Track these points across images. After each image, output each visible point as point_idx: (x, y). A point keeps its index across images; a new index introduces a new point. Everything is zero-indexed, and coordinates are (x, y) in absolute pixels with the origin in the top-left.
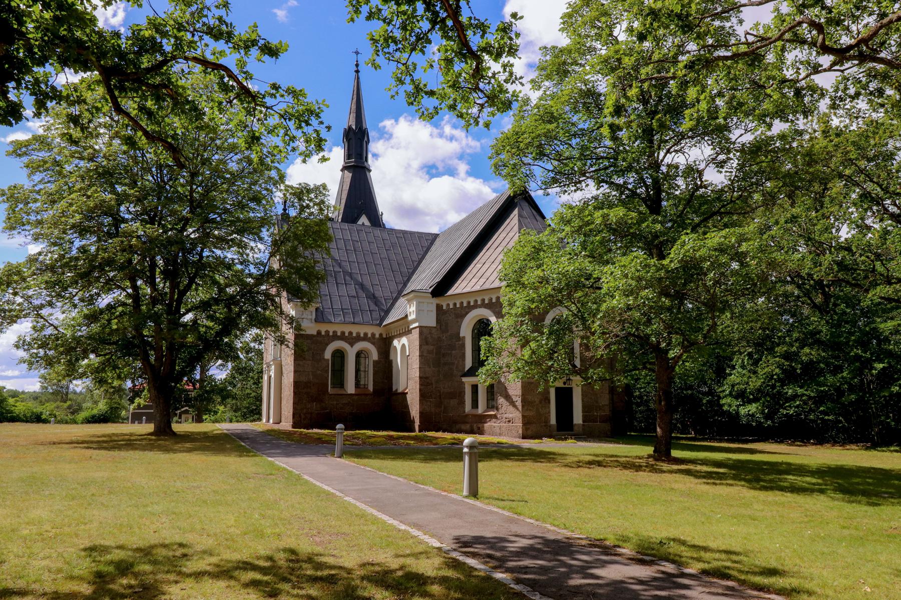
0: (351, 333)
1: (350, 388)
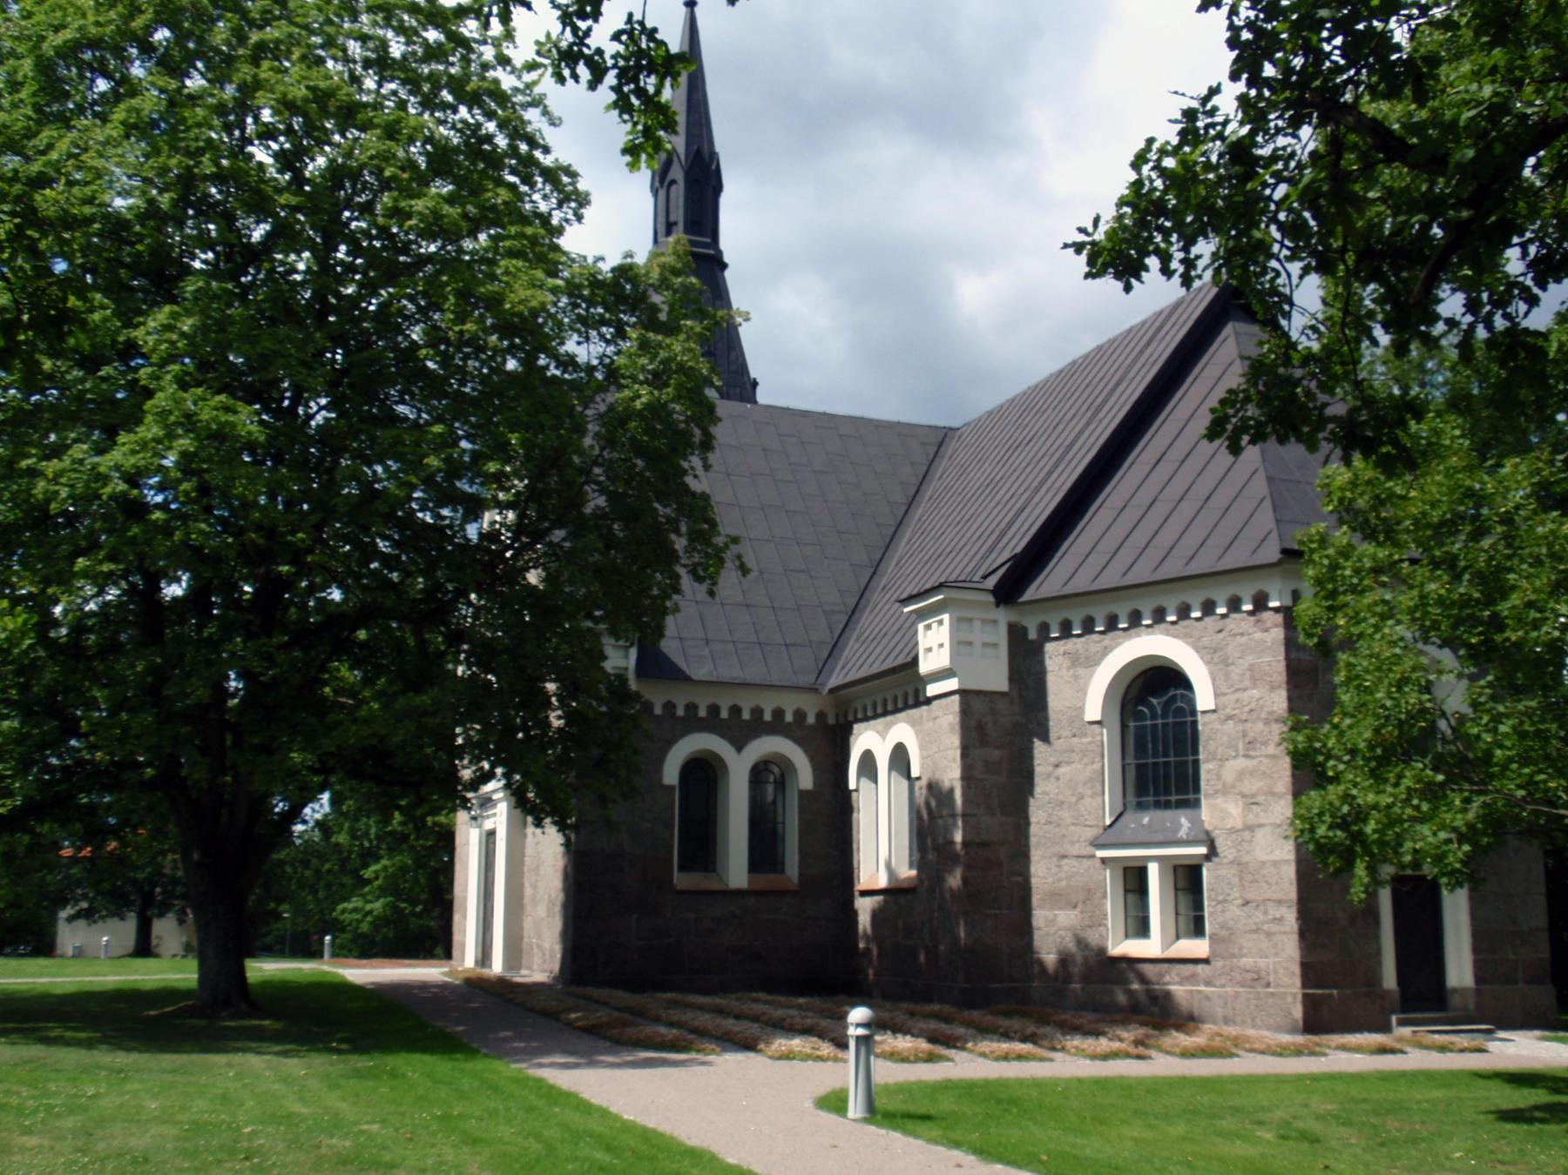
0: (736, 710)
1: (736, 870)
